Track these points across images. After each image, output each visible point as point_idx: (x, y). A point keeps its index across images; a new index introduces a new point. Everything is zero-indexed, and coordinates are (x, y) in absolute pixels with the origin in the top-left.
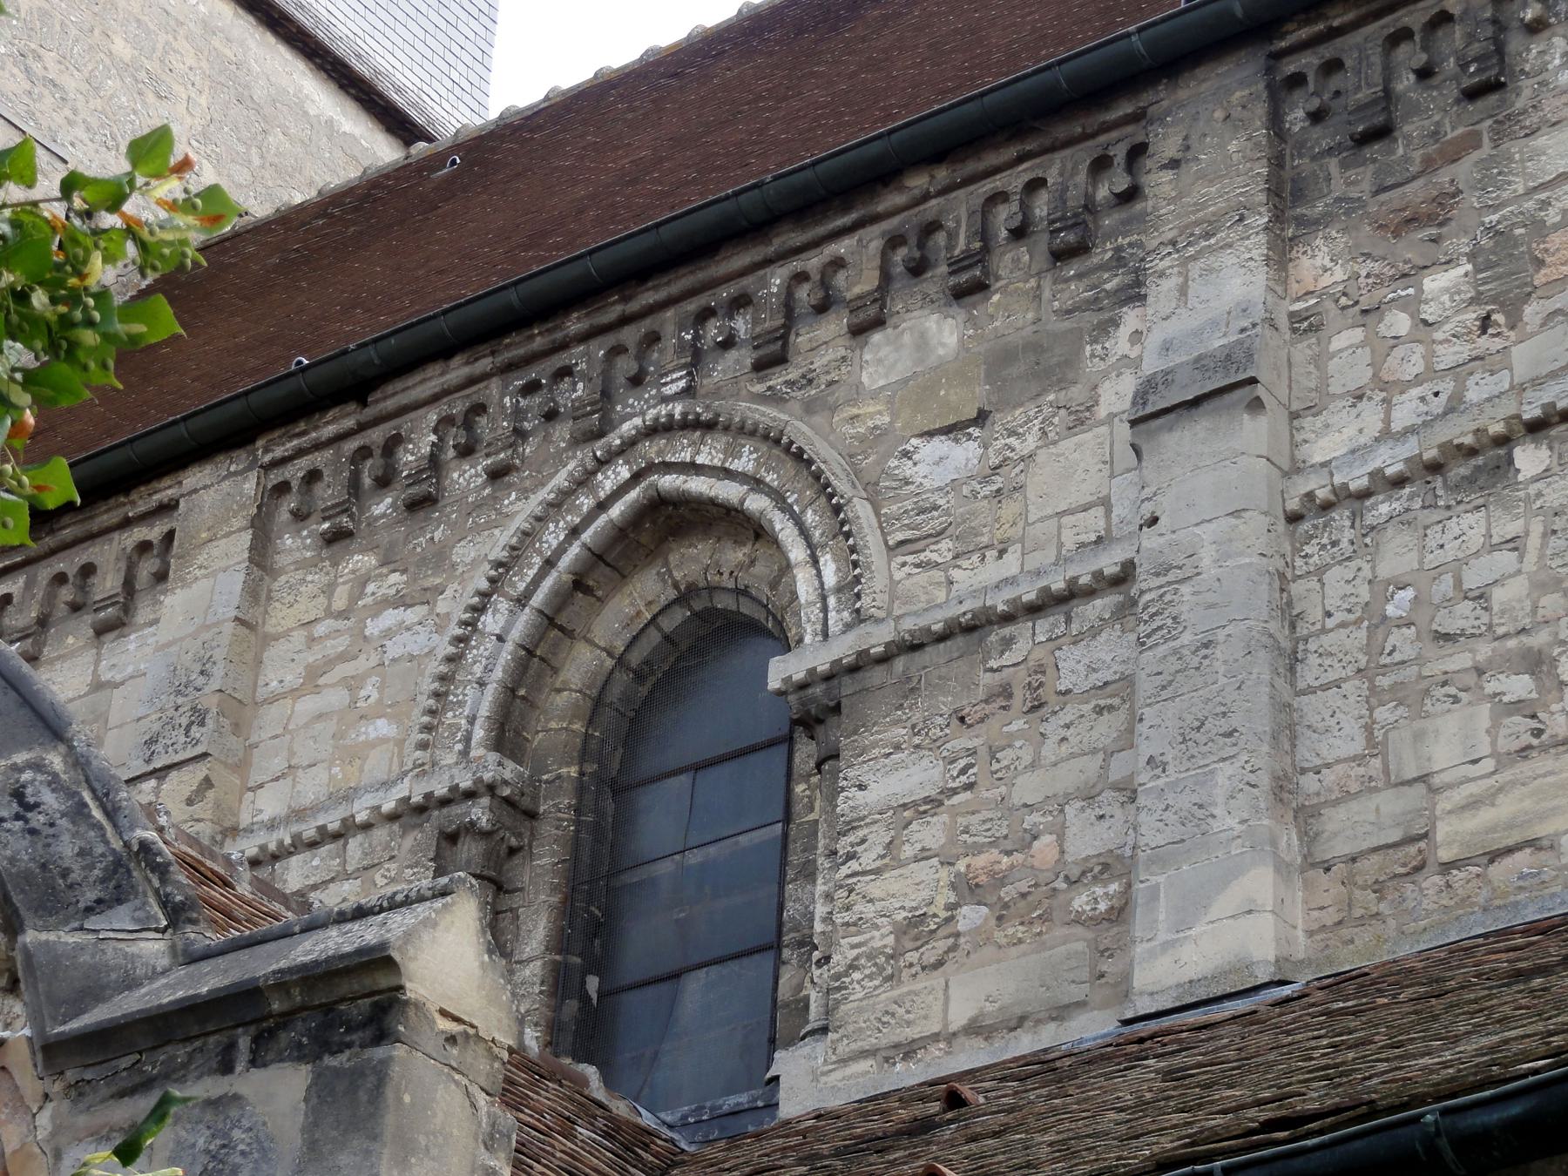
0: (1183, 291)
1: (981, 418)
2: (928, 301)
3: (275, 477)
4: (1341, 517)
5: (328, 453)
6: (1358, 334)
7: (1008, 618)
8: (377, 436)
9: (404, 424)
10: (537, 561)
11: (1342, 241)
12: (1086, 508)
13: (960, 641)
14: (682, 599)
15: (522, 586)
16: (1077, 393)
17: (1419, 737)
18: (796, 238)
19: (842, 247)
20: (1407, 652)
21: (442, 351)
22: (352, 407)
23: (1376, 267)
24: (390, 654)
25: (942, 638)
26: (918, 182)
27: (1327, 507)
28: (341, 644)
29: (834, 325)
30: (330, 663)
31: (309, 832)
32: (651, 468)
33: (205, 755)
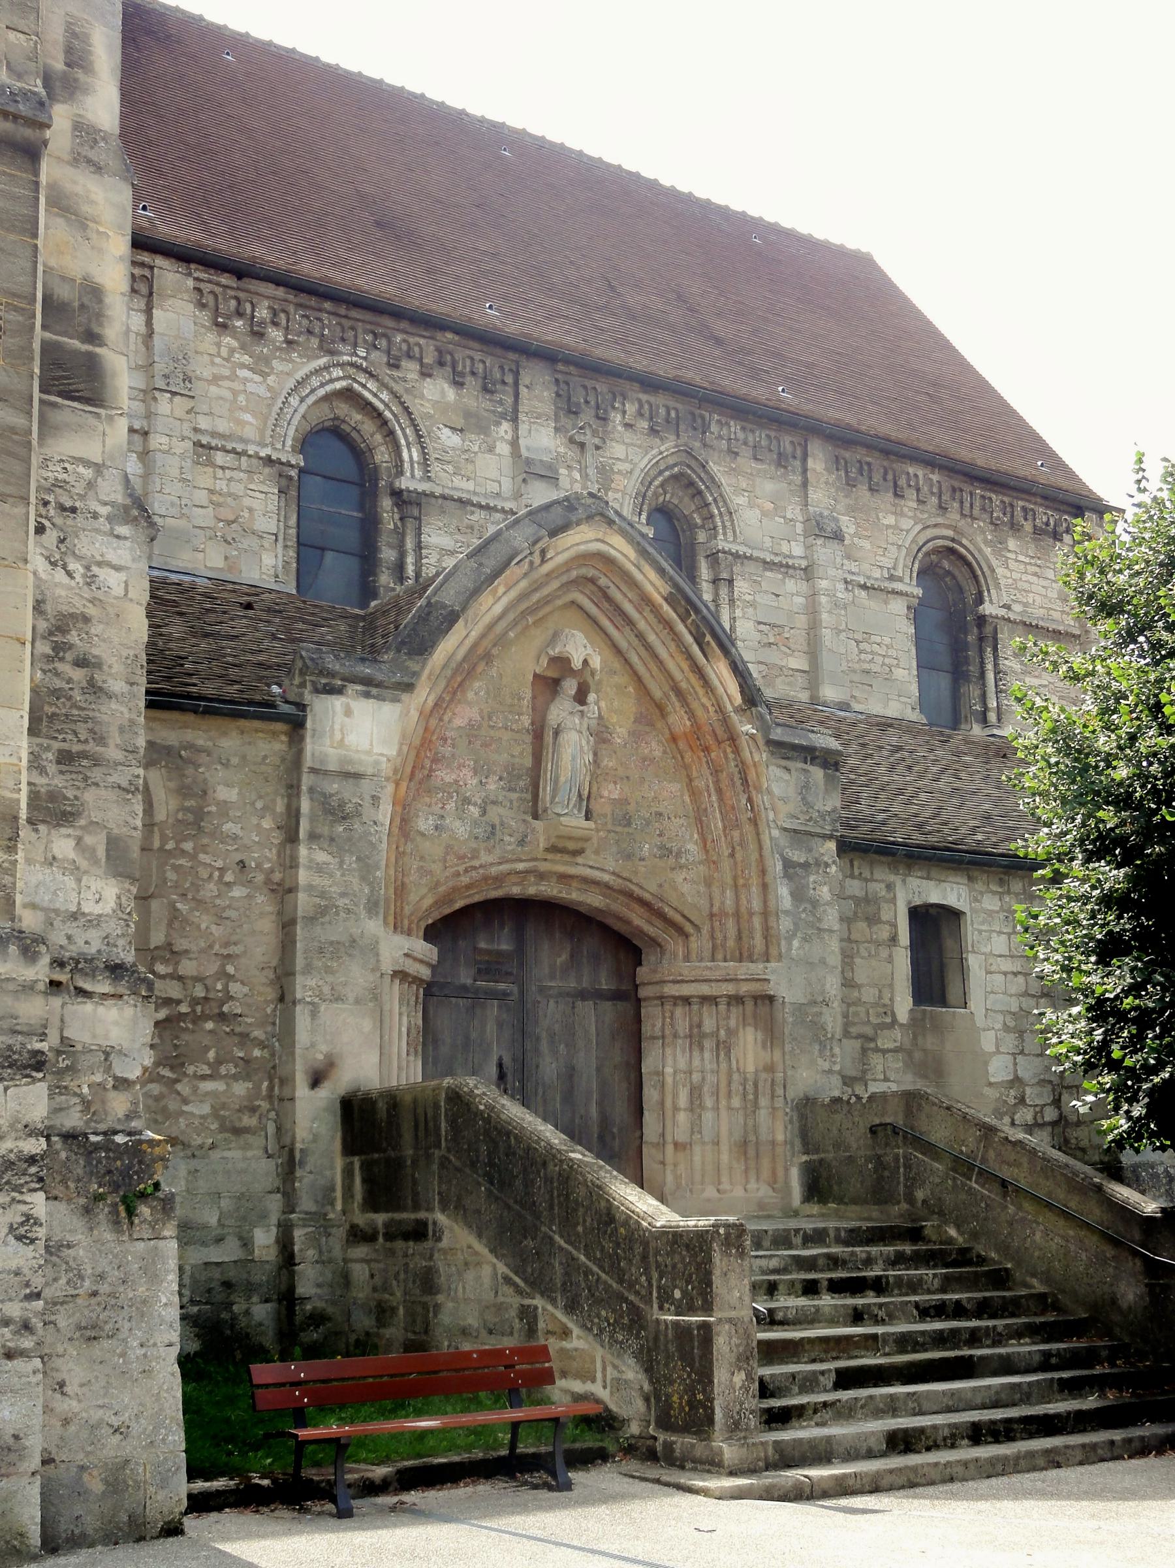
1: (461, 430)
2: (444, 378)
7: (473, 505)
13: (458, 504)
14: (333, 420)
18: (410, 330)
19: (422, 341)
25: (454, 500)
28: (227, 373)
31: (229, 447)
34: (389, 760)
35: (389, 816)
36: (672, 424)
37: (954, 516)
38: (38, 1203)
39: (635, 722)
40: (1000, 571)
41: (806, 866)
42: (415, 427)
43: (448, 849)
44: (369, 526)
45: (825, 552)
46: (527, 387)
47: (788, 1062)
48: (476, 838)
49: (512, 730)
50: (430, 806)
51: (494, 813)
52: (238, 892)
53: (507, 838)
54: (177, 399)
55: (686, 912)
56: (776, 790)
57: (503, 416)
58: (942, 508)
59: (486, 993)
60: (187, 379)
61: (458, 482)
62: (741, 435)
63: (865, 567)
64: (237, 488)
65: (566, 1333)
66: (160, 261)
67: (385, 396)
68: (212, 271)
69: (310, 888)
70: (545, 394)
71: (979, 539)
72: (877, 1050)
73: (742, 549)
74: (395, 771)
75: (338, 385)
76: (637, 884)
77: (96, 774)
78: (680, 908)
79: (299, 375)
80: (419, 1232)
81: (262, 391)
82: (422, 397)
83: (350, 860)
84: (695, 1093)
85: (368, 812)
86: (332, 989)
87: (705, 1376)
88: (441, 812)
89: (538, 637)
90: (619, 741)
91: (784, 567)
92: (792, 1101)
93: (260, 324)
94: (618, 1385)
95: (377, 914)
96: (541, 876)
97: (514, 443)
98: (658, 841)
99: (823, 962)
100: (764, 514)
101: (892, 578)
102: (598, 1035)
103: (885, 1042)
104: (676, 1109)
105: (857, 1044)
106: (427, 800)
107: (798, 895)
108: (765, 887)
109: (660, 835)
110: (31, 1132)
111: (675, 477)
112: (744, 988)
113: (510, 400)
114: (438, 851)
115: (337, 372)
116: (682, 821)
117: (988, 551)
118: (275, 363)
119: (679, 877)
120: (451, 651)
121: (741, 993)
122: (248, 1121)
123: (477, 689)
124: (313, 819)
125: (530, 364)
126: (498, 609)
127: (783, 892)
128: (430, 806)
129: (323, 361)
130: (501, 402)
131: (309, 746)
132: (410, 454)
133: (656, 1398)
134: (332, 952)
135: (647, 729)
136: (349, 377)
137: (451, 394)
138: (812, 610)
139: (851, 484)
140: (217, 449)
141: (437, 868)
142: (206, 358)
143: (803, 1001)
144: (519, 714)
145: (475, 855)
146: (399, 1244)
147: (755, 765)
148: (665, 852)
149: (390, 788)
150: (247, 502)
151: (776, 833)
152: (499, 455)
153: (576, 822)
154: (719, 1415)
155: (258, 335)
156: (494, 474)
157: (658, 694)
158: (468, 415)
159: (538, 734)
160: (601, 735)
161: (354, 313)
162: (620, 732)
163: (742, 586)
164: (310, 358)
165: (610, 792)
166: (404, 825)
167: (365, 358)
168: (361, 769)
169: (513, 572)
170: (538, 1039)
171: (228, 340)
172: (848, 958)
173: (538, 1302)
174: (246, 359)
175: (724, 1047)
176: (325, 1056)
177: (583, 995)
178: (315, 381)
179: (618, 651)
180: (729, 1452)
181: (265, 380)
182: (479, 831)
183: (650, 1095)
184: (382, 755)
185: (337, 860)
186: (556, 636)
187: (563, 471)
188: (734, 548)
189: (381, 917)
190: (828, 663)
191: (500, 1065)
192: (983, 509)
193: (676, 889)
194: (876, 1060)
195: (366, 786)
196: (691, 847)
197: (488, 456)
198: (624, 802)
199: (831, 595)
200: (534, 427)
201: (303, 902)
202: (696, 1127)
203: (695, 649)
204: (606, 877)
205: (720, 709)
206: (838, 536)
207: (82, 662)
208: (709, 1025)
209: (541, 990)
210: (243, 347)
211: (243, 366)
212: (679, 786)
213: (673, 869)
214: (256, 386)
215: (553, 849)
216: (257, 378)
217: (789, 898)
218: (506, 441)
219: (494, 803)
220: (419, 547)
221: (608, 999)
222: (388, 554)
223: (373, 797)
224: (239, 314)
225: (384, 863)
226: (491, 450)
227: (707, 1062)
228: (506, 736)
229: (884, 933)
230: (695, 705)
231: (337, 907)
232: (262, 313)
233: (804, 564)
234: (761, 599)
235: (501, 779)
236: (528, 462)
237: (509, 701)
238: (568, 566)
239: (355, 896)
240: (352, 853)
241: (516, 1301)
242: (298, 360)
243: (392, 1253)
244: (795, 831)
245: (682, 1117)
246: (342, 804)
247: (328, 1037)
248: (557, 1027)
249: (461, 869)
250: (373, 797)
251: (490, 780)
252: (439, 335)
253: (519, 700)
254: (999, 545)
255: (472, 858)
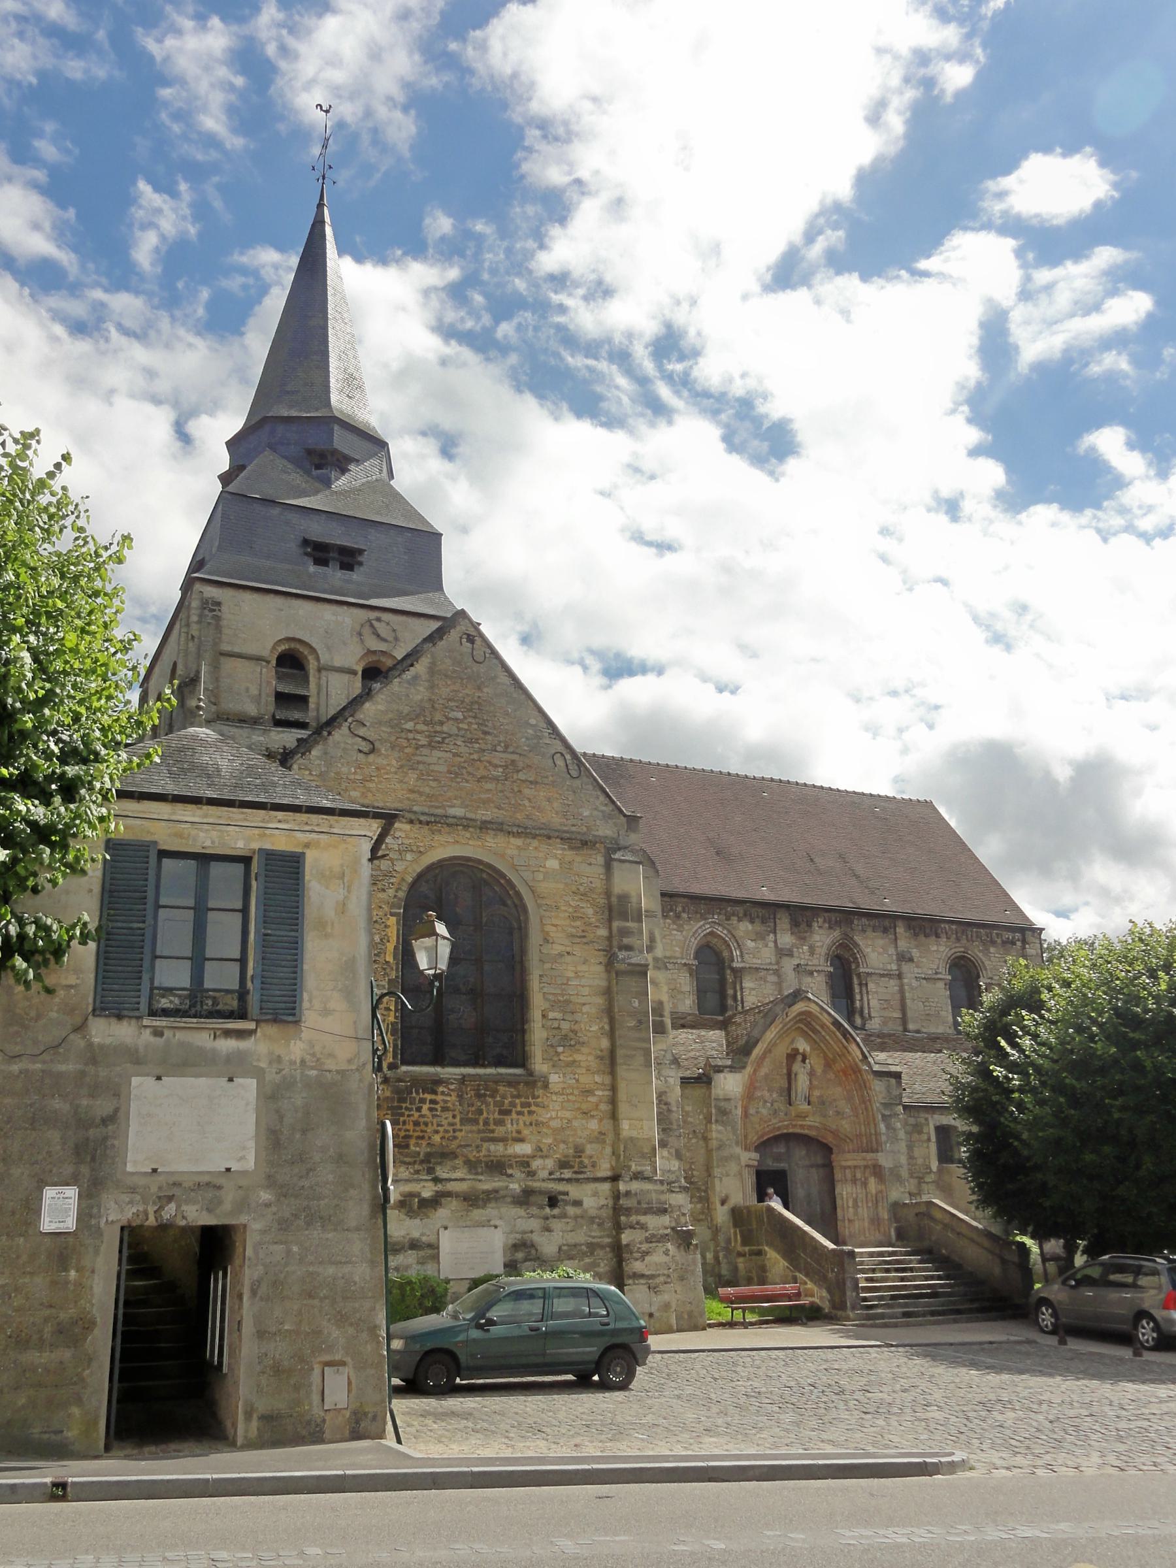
29: (736, 918)
36: (838, 923)
37: (964, 941)
38: (669, 1245)
40: (987, 963)
41: (890, 1116)
42: (738, 943)
44: (722, 982)
45: (906, 968)
51: (776, 1105)
52: (694, 1141)
56: (877, 1088)
57: (770, 932)
58: (958, 940)
61: (755, 961)
62: (867, 923)
63: (925, 970)
64: (675, 976)
65: (806, 1283)
67: (725, 932)
69: (717, 1139)
71: (976, 951)
72: (924, 1182)
73: (870, 971)
77: (671, 1133)
79: (694, 930)
80: (759, 1253)
81: (681, 938)
83: (729, 1128)
84: (855, 1201)
87: (844, 1294)
89: (788, 1040)
91: (889, 976)
94: (821, 1298)
96: (794, 1126)
97: (775, 942)
99: (899, 1152)
100: (879, 954)
101: (937, 973)
103: (928, 1179)
104: (848, 1207)
105: (916, 1181)
107: (888, 1127)
108: (875, 1125)
110: (666, 1228)
111: (840, 944)
113: (772, 925)
117: (980, 955)
119: (844, 1122)
122: (702, 1217)
123: (767, 1062)
124: (716, 1115)
126: (772, 1036)
127: (882, 1127)
129: (702, 923)
131: (713, 1091)
132: (737, 953)
133: (832, 1301)
137: (750, 927)
138: (902, 992)
139: (916, 935)
141: (757, 1126)
146: (754, 1257)
148: (838, 1113)
150: (678, 981)
153: (805, 1107)
154: (848, 1304)
155: (678, 917)
159: (789, 1074)
160: (812, 1074)
162: (819, 1070)
163: (871, 986)
166: (746, 1114)
169: (777, 1022)
171: (668, 921)
172: (910, 1148)
173: (797, 1274)
174: (675, 927)
175: (865, 1184)
177: (812, 1166)
180: (851, 1315)
183: (839, 1202)
186: (793, 1041)
187: (795, 950)
188: (867, 970)
190: (909, 1014)
192: (977, 937)
194: (924, 1186)
196: (847, 1110)
198: (821, 1096)
199: (910, 985)
201: (714, 1144)
202: (856, 1213)
203: (844, 1041)
205: (854, 1061)
206: (911, 960)
207: (666, 1104)
208: (859, 1175)
210: (674, 923)
214: (678, 936)
215: (797, 1116)
220: (742, 989)
222: (730, 992)
224: (671, 910)
226: (766, 946)
228: (778, 1077)
229: (925, 1137)
232: (679, 909)
233: (897, 972)
234: (880, 990)
236: (782, 949)
238: (795, 1017)
241: (791, 1274)
243: (751, 1260)
245: (851, 1210)
254: (986, 952)
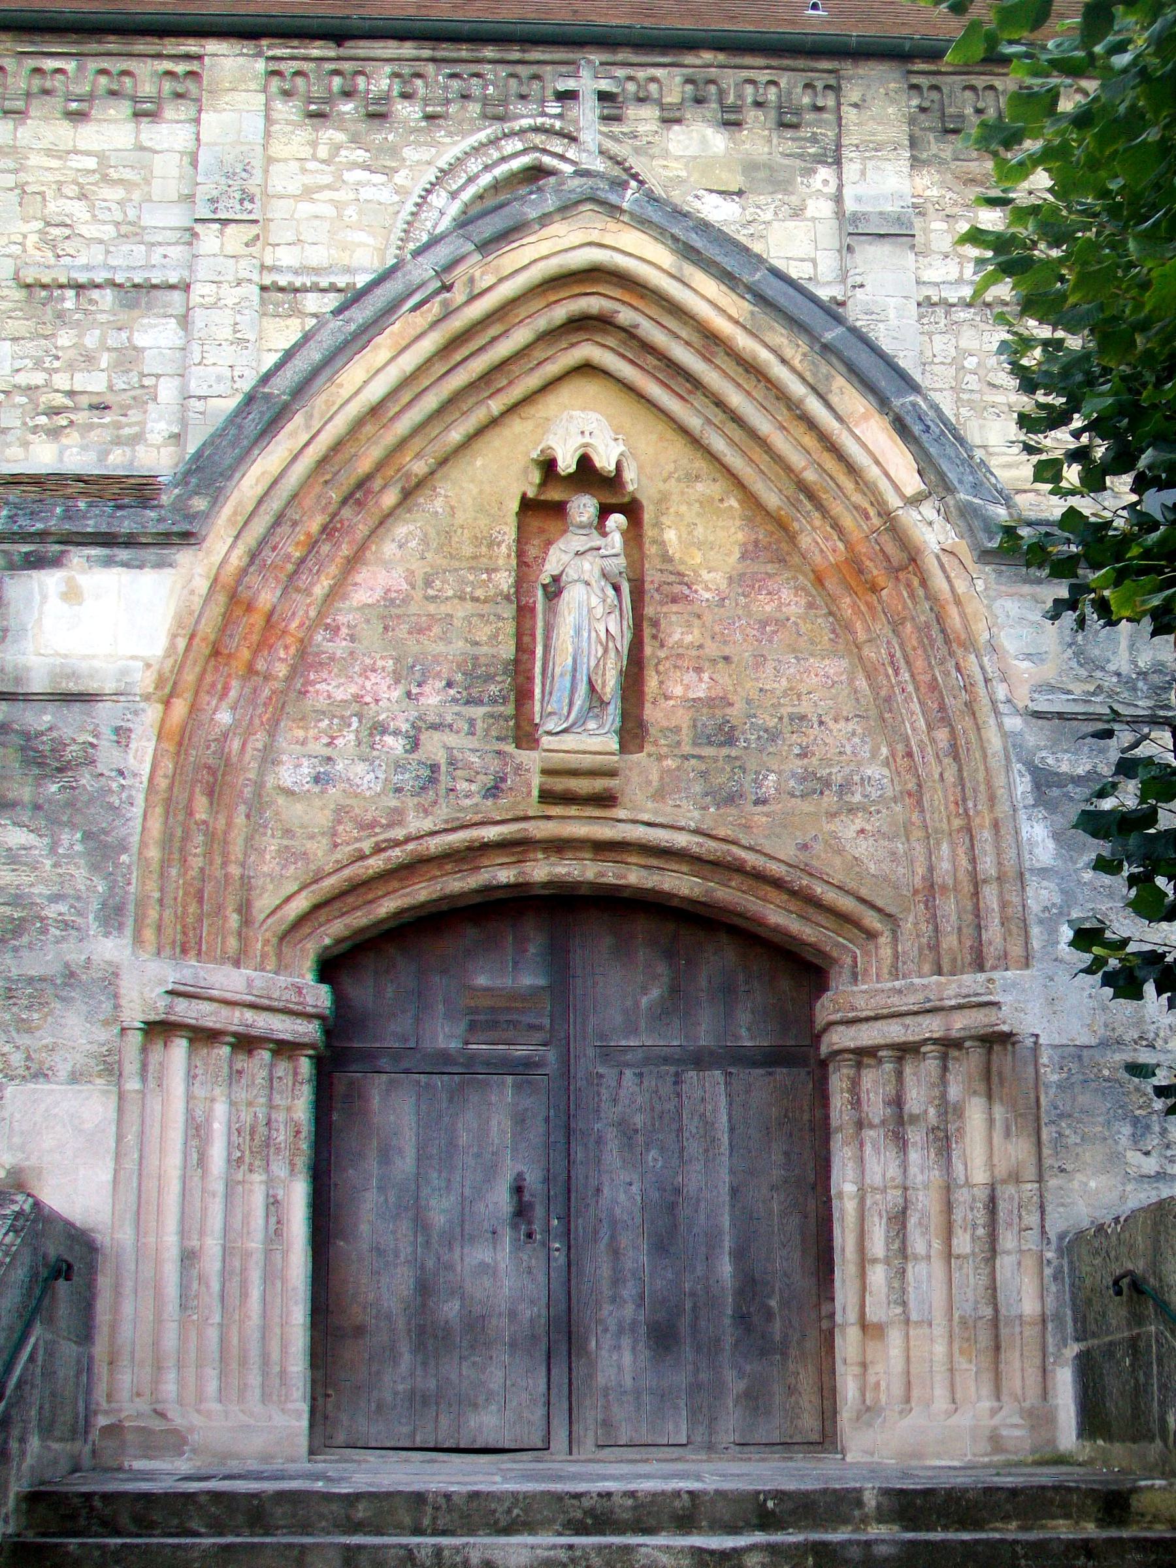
0: (863, 173)
1: (740, 193)
2: (705, 120)
3: (274, 66)
4: (940, 311)
5: (312, 65)
6: (944, 226)
8: (347, 66)
9: (369, 67)
10: (464, 177)
11: (937, 177)
12: (802, 260)
15: (455, 187)
16: (794, 200)
17: (981, 427)
19: (659, 72)
20: (975, 387)
21: (402, 36)
22: (332, 45)
23: (955, 196)
24: (362, 197)
26: (708, 56)
27: (934, 305)
28: (327, 179)
29: (650, 113)
30: (321, 188)
31: (324, 284)
32: (535, 148)
33: (256, 221)
34: (148, 666)
35: (148, 759)
39: (743, 557)
43: (341, 812)
46: (856, 106)
47: (1047, 1162)
48: (399, 790)
49: (475, 600)
50: (304, 743)
51: (434, 746)
53: (462, 786)
54: (231, 229)
55: (864, 892)
57: (820, 160)
59: (488, 1064)
60: (247, 197)
66: (212, 46)
68: (295, 43)
70: (890, 110)
74: (160, 682)
75: (516, 164)
76: (750, 848)
78: (851, 885)
81: (386, 195)
82: (666, 154)
83: (70, 839)
85: (108, 756)
86: (29, 1058)
88: (328, 752)
90: (707, 595)
92: (1061, 1237)
93: (378, 101)
95: (121, 927)
98: (797, 765)
102: (732, 1130)
106: (300, 734)
109: (803, 755)
112: (960, 1023)
114: (322, 818)
115: (516, 145)
116: (851, 726)
118: (407, 152)
119: (848, 829)
120: (275, 470)
121: (954, 1034)
125: (861, 71)
128: (304, 743)
130: (814, 139)
134: (30, 996)
135: (770, 568)
136: (535, 148)
137: (718, 141)
140: (304, 289)
142: (294, 166)
143: (1084, 1039)
144: (489, 571)
145: (396, 817)
147: (958, 602)
149: (152, 713)
151: (1014, 723)
152: (813, 219)
156: (806, 250)
157: (772, 500)
158: (750, 167)
161: (536, 54)
164: (464, 134)
165: (687, 687)
167: (560, 116)
168: (93, 686)
170: (599, 1141)
174: (360, 155)
176: (9, 1172)
177: (699, 1060)
178: (474, 166)
179: (695, 441)
181: (390, 180)
182: (405, 779)
184: (133, 658)
185: (46, 840)
189: (129, 931)
191: (518, 1190)
193: (840, 851)
195: (105, 712)
196: (874, 771)
197: (791, 224)
200: (870, 164)
204: (681, 840)
208: (917, 1098)
209: (607, 1054)
210: (355, 139)
211: (354, 165)
212: (844, 663)
213: (833, 815)
214: (378, 190)
216: (379, 178)
217: (1051, 844)
218: (824, 195)
219: (435, 727)
221: (755, 1064)
223: (118, 730)
224: (347, 94)
225: (135, 839)
227: (913, 1170)
228: (461, 611)
230: (837, 509)
231: (42, 919)
235: (449, 685)
236: (856, 218)
237: (468, 550)
239: (79, 898)
240: (73, 826)
242: (448, 140)
244: (1060, 715)
246: (59, 746)
247: (17, 1140)
248: (639, 1120)
249: (367, 846)
250: (118, 730)
251: (427, 689)
252: (689, 59)
253: (490, 546)
255: (390, 826)
